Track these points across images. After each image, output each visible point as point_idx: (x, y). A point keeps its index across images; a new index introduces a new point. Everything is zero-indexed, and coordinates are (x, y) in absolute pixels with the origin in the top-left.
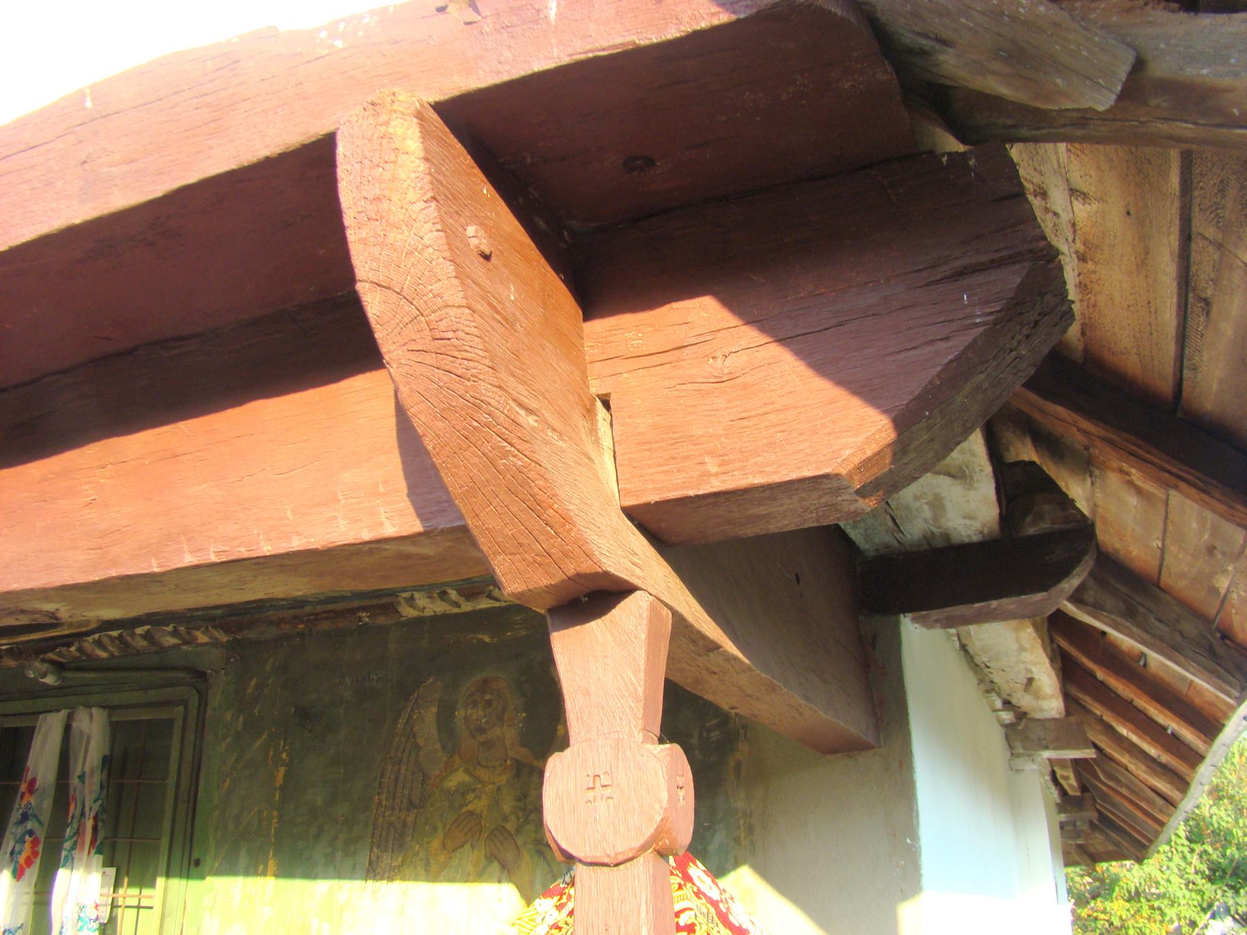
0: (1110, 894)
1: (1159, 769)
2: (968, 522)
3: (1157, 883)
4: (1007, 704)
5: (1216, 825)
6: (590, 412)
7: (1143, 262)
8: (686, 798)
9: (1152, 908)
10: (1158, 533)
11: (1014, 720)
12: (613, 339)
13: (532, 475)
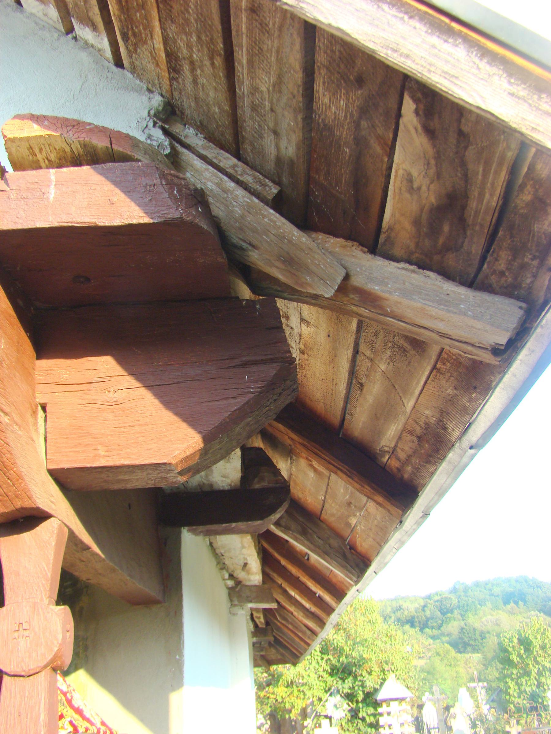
0: (277, 684)
1: (310, 615)
2: (224, 479)
3: (303, 677)
4: (231, 576)
5: (336, 645)
6: (35, 413)
7: (333, 359)
8: (70, 636)
9: (299, 691)
10: (323, 492)
11: (234, 585)
12: (52, 372)
13: (4, 450)
